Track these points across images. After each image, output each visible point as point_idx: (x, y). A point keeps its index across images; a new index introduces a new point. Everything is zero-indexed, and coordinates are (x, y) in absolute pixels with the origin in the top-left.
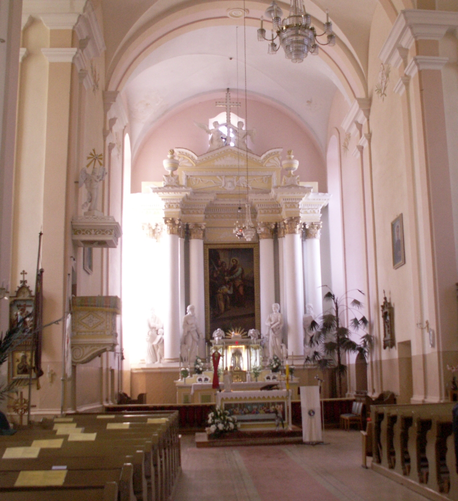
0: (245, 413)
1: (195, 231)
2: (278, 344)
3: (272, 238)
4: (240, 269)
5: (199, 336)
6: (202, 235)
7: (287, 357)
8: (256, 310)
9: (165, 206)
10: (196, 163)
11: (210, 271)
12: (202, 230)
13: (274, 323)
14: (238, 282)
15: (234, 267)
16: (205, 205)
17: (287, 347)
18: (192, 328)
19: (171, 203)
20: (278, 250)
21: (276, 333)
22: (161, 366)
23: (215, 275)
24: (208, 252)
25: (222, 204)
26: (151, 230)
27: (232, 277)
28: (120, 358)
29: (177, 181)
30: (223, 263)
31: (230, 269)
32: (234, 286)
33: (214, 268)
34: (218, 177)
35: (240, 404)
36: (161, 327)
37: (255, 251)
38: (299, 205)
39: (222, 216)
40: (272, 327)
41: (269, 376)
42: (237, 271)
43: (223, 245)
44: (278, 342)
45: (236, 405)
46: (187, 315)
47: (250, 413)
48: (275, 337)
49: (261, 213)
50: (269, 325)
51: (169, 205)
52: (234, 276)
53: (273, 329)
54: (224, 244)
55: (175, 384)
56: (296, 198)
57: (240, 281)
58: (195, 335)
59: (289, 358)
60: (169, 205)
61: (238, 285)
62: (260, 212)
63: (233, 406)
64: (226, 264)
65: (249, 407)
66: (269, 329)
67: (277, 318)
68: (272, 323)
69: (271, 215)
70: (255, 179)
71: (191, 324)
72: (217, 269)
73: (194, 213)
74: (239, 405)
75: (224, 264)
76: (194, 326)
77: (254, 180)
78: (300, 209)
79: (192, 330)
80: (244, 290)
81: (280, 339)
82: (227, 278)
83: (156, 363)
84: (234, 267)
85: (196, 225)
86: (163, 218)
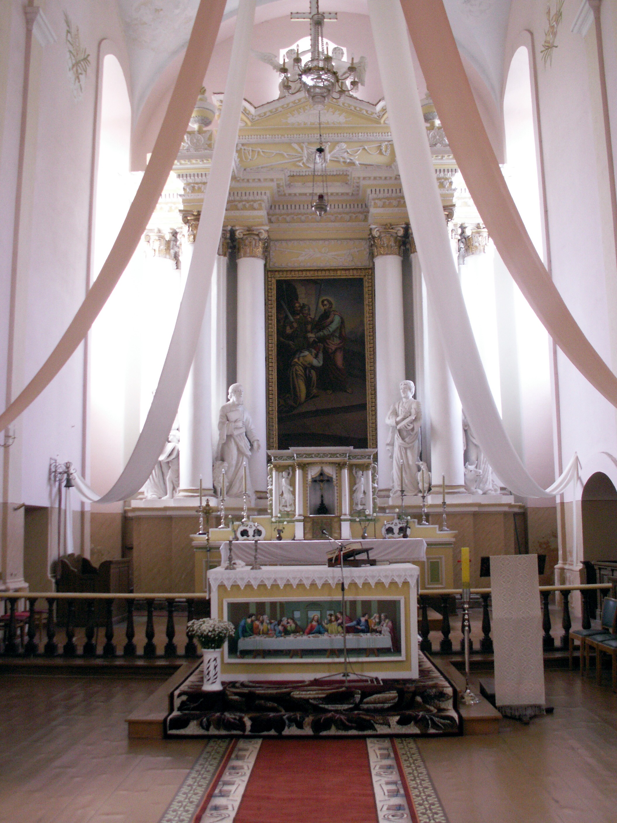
0: (286, 632)
1: (247, 242)
2: (410, 462)
3: (399, 255)
4: (337, 319)
5: (252, 445)
6: (260, 250)
7: (430, 489)
8: (369, 397)
9: (184, 189)
10: (252, 120)
11: (278, 321)
12: (260, 240)
13: (403, 419)
14: (334, 344)
15: (326, 315)
16: (268, 194)
17: (429, 469)
18: (237, 428)
19: (197, 183)
20: (412, 282)
21: (407, 440)
22: (172, 504)
23: (289, 331)
24: (274, 286)
25: (300, 194)
26: (163, 242)
27: (321, 333)
28: (64, 484)
29: (209, 142)
30: (303, 307)
31: (317, 319)
32: (325, 352)
33: (286, 317)
34: (296, 146)
35: (273, 605)
36: (177, 428)
37: (366, 284)
38: (451, 183)
39: (303, 218)
40: (398, 427)
41: (393, 526)
42: (332, 322)
43: (304, 273)
44: (412, 458)
45: (261, 606)
46: (229, 402)
47: (298, 630)
48: (406, 449)
49: (376, 206)
50: (394, 424)
51: (193, 187)
52: (326, 332)
53: (400, 431)
54: (307, 270)
55: (192, 540)
56: (446, 167)
57: (337, 341)
58: (244, 444)
59: (433, 489)
60: (193, 187)
61: (333, 348)
62: (375, 203)
63: (253, 610)
64: (309, 309)
65: (297, 615)
66: (393, 433)
67: (410, 408)
68: (398, 419)
69: (396, 210)
70: (366, 147)
71: (235, 421)
72: (292, 319)
73: (244, 208)
74: (268, 609)
75: (306, 308)
76: (240, 424)
77: (364, 149)
78: (455, 190)
79: (236, 433)
80: (345, 358)
81: (416, 452)
82: (311, 336)
83: (164, 498)
84: (326, 315)
85: (250, 231)
86: (180, 211)
